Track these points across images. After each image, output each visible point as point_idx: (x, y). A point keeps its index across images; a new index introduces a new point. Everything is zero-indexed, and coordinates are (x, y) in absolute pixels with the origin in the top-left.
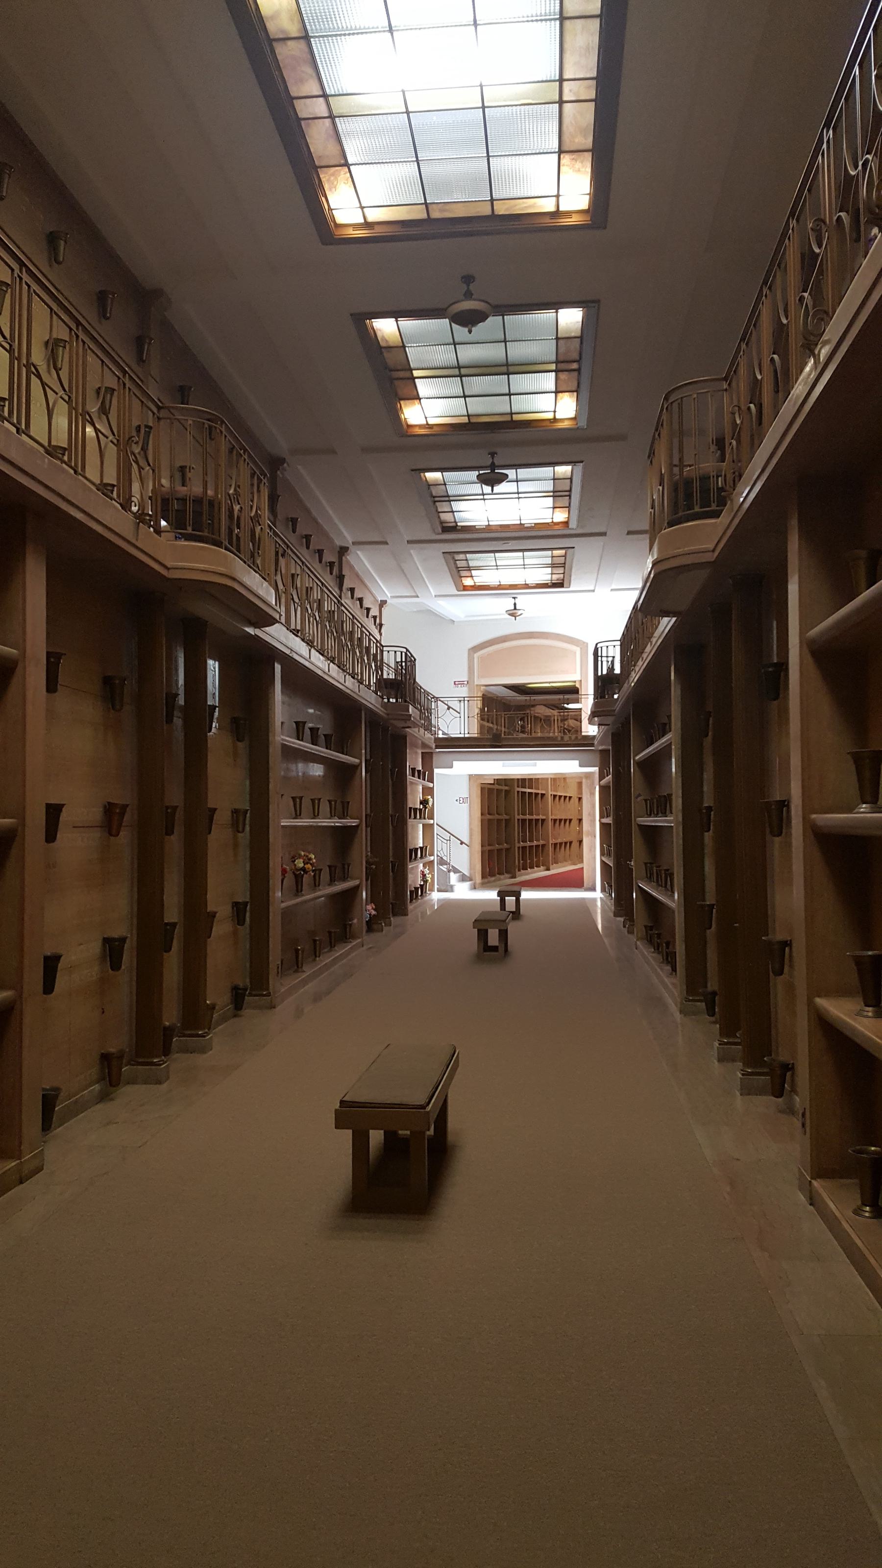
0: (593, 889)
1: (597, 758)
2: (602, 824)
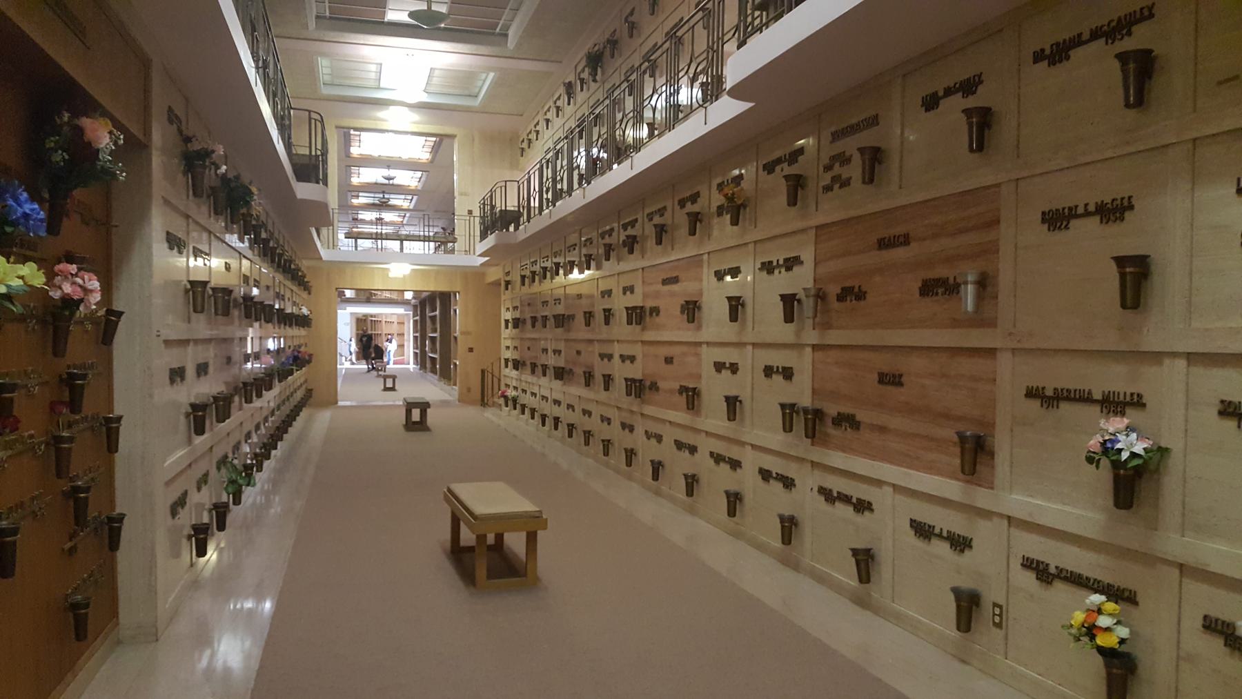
0: (409, 364)
1: (412, 308)
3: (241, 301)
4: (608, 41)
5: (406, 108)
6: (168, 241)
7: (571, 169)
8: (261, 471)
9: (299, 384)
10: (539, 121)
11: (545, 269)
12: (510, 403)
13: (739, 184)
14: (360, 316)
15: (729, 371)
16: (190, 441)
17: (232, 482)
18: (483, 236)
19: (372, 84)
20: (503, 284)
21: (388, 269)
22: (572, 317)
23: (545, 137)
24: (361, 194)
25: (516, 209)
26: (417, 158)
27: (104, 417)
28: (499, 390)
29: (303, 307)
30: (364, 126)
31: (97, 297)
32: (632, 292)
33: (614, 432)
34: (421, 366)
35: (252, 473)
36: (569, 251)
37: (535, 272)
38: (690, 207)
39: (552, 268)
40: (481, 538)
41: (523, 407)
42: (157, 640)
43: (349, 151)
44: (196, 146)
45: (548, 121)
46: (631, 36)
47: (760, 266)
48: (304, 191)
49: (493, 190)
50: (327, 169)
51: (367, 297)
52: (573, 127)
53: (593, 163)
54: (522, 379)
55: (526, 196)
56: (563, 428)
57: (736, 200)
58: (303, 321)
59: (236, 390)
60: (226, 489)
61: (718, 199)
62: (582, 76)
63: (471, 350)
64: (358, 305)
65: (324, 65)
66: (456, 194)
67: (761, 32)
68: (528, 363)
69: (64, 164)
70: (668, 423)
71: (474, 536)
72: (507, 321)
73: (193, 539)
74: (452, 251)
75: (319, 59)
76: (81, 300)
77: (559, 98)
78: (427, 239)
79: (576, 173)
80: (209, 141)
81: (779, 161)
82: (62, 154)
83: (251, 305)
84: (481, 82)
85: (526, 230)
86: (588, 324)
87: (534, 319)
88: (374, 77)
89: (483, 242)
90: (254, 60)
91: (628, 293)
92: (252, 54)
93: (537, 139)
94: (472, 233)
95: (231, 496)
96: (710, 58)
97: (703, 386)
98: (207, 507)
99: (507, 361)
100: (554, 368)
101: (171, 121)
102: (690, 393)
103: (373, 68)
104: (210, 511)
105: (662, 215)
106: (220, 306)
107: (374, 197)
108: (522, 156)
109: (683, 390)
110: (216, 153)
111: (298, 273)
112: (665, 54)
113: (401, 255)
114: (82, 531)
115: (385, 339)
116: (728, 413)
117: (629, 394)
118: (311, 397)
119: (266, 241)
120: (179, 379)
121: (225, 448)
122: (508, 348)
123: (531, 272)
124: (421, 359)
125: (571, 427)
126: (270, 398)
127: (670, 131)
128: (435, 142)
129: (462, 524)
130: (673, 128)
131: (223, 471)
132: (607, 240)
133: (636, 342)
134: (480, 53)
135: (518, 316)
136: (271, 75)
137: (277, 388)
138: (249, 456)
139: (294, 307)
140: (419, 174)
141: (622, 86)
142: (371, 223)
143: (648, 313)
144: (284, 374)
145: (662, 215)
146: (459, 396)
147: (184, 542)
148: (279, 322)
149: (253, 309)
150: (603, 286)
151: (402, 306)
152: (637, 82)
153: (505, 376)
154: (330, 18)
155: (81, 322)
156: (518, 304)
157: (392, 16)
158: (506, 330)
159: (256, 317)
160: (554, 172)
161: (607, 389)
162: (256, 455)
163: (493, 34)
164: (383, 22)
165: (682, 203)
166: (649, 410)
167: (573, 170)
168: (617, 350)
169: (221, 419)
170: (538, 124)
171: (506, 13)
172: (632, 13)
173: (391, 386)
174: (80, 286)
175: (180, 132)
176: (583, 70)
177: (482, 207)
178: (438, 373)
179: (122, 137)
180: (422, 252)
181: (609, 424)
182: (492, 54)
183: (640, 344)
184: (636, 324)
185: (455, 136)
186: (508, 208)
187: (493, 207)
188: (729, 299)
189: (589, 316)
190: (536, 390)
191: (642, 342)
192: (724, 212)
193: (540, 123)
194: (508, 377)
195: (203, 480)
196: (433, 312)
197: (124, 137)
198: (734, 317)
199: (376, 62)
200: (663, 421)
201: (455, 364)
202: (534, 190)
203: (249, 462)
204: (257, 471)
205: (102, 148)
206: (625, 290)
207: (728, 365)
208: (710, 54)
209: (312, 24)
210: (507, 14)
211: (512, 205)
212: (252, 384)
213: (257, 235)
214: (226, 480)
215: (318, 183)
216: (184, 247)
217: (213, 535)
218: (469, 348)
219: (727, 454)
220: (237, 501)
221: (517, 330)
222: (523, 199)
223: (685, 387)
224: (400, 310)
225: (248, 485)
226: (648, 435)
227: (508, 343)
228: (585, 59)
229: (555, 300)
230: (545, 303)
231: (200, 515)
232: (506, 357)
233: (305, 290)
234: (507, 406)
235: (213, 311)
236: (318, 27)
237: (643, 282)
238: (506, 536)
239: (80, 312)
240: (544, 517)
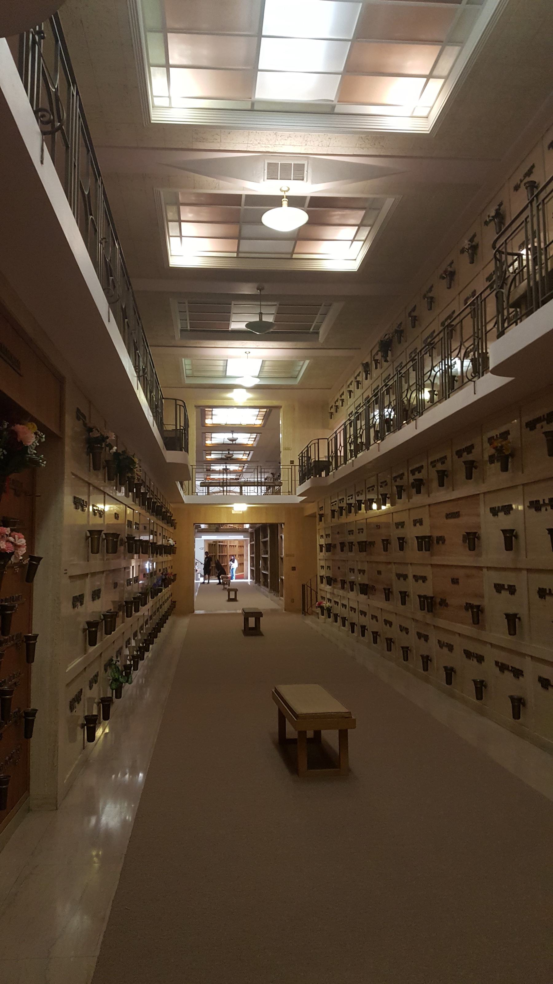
0: (247, 579)
1: (249, 535)
2: (251, 557)
3: (126, 540)
4: (396, 331)
5: (245, 390)
6: (75, 503)
7: (368, 428)
8: (137, 670)
9: (166, 598)
10: (343, 392)
11: (350, 505)
12: (325, 612)
13: (506, 439)
14: (212, 542)
15: (508, 592)
16: (85, 651)
17: (115, 680)
18: (302, 481)
19: (221, 374)
20: (318, 516)
21: (232, 508)
22: (372, 544)
23: (349, 403)
24: (212, 452)
25: (327, 459)
26: (253, 423)
27: (25, 636)
28: (317, 601)
29: (170, 539)
30: (215, 404)
31: (23, 550)
32: (421, 524)
33: (411, 640)
34: (256, 580)
35: (130, 672)
36: (369, 491)
37: (343, 507)
38: (466, 457)
39: (355, 504)
40: (302, 734)
41: (336, 616)
42: (57, 809)
43: (205, 422)
44: (95, 434)
45: (350, 392)
46: (414, 326)
47: (529, 505)
48: (171, 456)
49: (309, 446)
50: (188, 439)
51: (217, 528)
52: (370, 397)
53: (385, 421)
54: (335, 593)
55: (333, 450)
56: (369, 635)
57: (504, 451)
58: (169, 550)
59: (120, 607)
60: (111, 685)
61: (489, 451)
62: (376, 358)
63: (294, 569)
64: (210, 534)
65: (186, 364)
66: (281, 449)
67: (516, 325)
68: (339, 579)
69: (4, 458)
70: (457, 635)
71: (297, 733)
72: (321, 546)
73: (86, 727)
74: (278, 493)
75: (183, 359)
76: (13, 553)
77: (358, 375)
78: (259, 484)
79: (372, 430)
80: (105, 430)
81: (539, 420)
82: (2, 451)
83: (133, 543)
84: (300, 367)
85: (335, 475)
86: (386, 549)
87: (342, 545)
88: (222, 364)
89: (302, 485)
90: (136, 372)
91: (418, 524)
92: (134, 367)
93: (342, 406)
94: (293, 479)
95: (114, 691)
96: (476, 343)
97: (486, 603)
98: (96, 701)
99: (322, 577)
100: (360, 584)
101: (78, 418)
102: (475, 610)
103: (221, 363)
104: (98, 704)
105: (443, 463)
106: (110, 547)
107: (222, 454)
108: (331, 418)
109: (469, 606)
110: (110, 438)
111: (167, 514)
112: (440, 342)
113: (241, 499)
114: (6, 724)
115: (229, 560)
116: (509, 629)
117: (422, 609)
118: (175, 607)
119: (145, 494)
120: (79, 604)
121: (111, 653)
122: (322, 567)
123: (339, 507)
124: (256, 574)
125: (375, 635)
126: (145, 611)
127: (446, 399)
128: (266, 412)
129: (287, 722)
130: (449, 397)
131: (109, 671)
132: (399, 482)
133: (427, 565)
134: (298, 347)
135: (330, 542)
136: (149, 379)
137: (151, 602)
138: (128, 658)
139: (164, 540)
140: (254, 436)
141: (408, 365)
142: (219, 472)
143: (435, 542)
144: (155, 591)
145: (443, 463)
146: (285, 606)
147: (79, 728)
148: (153, 553)
149: (134, 545)
150: (398, 518)
151: (243, 534)
152: (418, 363)
153: (321, 590)
154: (191, 330)
155: (12, 566)
156: (330, 533)
157: (234, 326)
158: (321, 553)
159: (136, 550)
160: (355, 430)
161: (404, 603)
162: (133, 658)
163: (308, 333)
164: (228, 331)
165: (459, 454)
166: (442, 623)
167: (370, 428)
168: (411, 571)
169: (108, 632)
170: (343, 394)
171: (317, 318)
172: (414, 310)
173: (234, 597)
174: (12, 543)
175: (85, 425)
176: (377, 354)
177: (300, 458)
178: (269, 587)
179: (44, 436)
180: (255, 494)
181: (407, 633)
182: (307, 347)
183: (430, 567)
184: (426, 550)
185: (281, 407)
186: (320, 459)
187: (309, 458)
188: (504, 531)
189: (386, 543)
190: (345, 602)
191: (431, 565)
192: (496, 461)
193: (345, 394)
194: (324, 591)
195: (94, 680)
196: (265, 538)
197: (45, 437)
198: (509, 546)
199: (223, 359)
200: (454, 633)
201: (282, 580)
202: (340, 445)
203: (128, 663)
204: (134, 670)
205: (30, 445)
206: (415, 522)
207: (506, 587)
208: (476, 340)
209: (178, 335)
210: (318, 318)
211: (323, 457)
212: (131, 602)
213: (138, 490)
214: (111, 678)
215: (181, 450)
216: (86, 506)
217: (100, 723)
218: (292, 567)
219: (510, 664)
220: (118, 696)
221: (330, 553)
222: (332, 452)
223: (470, 604)
224: (241, 537)
225: (127, 682)
226: (441, 644)
227: (323, 563)
228: (378, 346)
229: (359, 530)
230: (351, 532)
231: (90, 708)
232: (322, 575)
233: (171, 526)
234: (323, 615)
235: (105, 551)
236: (182, 337)
237: (430, 516)
238: (323, 732)
239: (12, 562)
240: (353, 717)
